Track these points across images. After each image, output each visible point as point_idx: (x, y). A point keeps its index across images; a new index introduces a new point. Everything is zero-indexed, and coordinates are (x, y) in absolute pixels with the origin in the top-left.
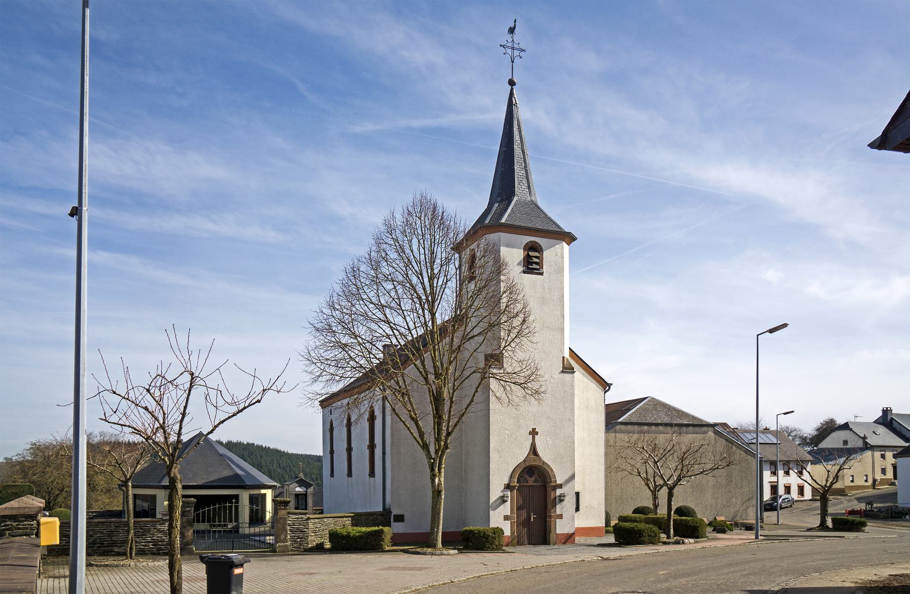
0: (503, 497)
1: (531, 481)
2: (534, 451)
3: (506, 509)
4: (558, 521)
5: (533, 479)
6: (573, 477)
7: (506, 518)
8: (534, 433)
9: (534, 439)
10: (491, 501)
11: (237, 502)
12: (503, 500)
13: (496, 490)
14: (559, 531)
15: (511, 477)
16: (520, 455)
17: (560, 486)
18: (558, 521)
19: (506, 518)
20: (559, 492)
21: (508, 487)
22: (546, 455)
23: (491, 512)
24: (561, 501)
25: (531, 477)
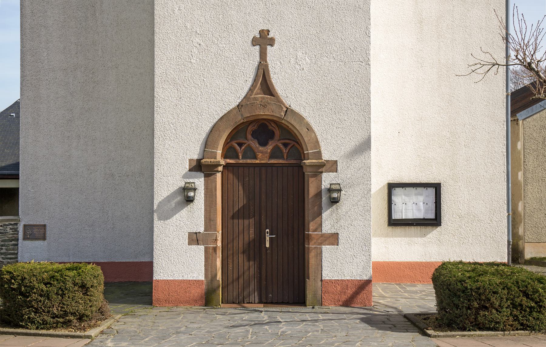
0: (185, 189)
1: (263, 155)
2: (263, 82)
3: (194, 218)
4: (326, 249)
5: (269, 148)
6: (365, 146)
7: (194, 239)
8: (263, 40)
9: (263, 55)
10: (156, 203)
11: (45, 229)
12: (186, 196)
13: (171, 167)
14: (328, 274)
15: (208, 143)
16: (228, 92)
17: (333, 166)
18: (326, 249)
19: (194, 239)
20: (327, 179)
21: (198, 167)
22: (296, 92)
23: (158, 224)
24: (334, 201)
25: (264, 144)
